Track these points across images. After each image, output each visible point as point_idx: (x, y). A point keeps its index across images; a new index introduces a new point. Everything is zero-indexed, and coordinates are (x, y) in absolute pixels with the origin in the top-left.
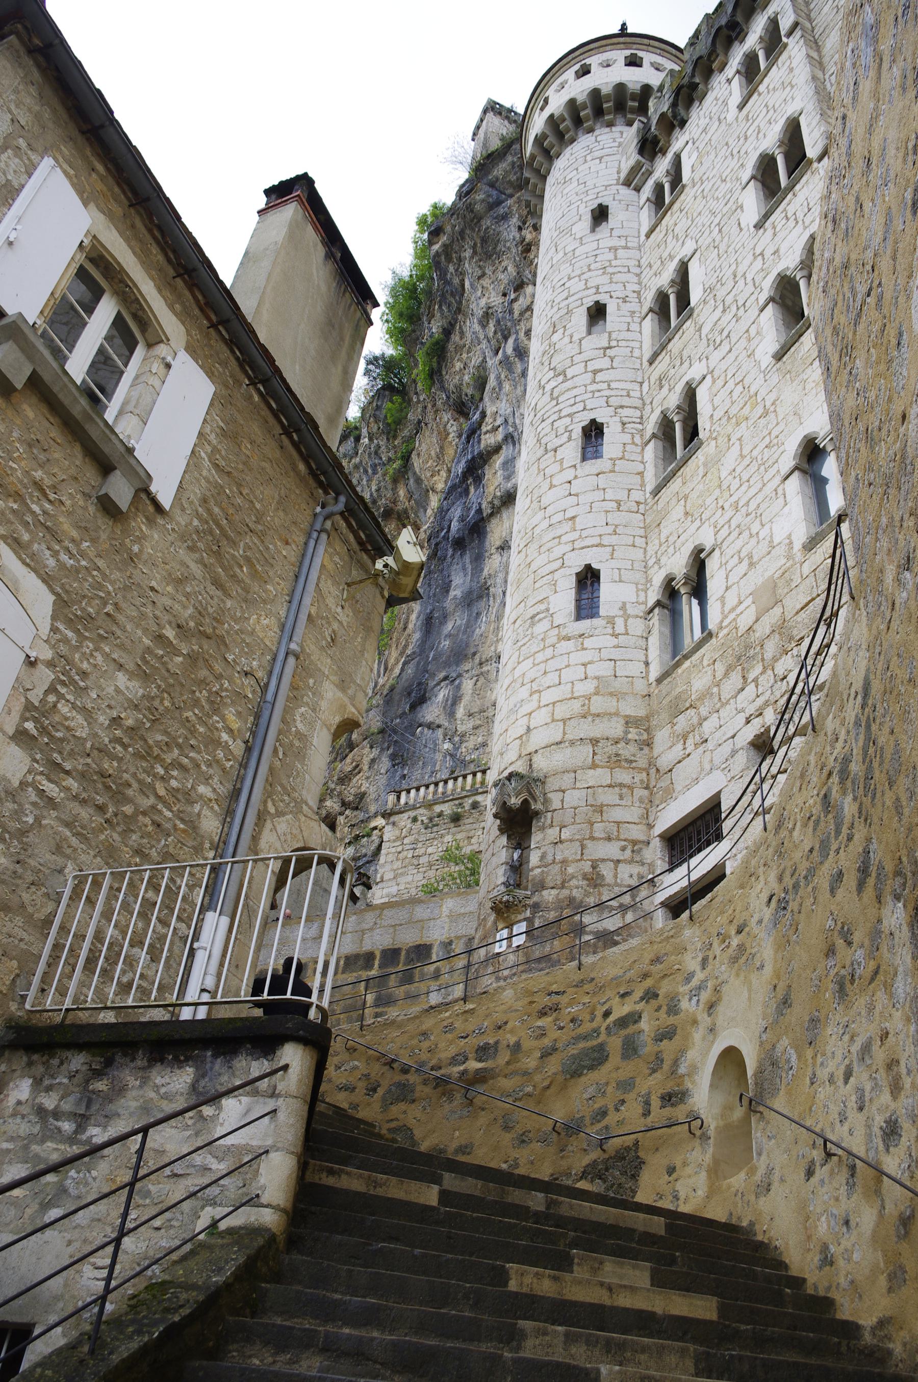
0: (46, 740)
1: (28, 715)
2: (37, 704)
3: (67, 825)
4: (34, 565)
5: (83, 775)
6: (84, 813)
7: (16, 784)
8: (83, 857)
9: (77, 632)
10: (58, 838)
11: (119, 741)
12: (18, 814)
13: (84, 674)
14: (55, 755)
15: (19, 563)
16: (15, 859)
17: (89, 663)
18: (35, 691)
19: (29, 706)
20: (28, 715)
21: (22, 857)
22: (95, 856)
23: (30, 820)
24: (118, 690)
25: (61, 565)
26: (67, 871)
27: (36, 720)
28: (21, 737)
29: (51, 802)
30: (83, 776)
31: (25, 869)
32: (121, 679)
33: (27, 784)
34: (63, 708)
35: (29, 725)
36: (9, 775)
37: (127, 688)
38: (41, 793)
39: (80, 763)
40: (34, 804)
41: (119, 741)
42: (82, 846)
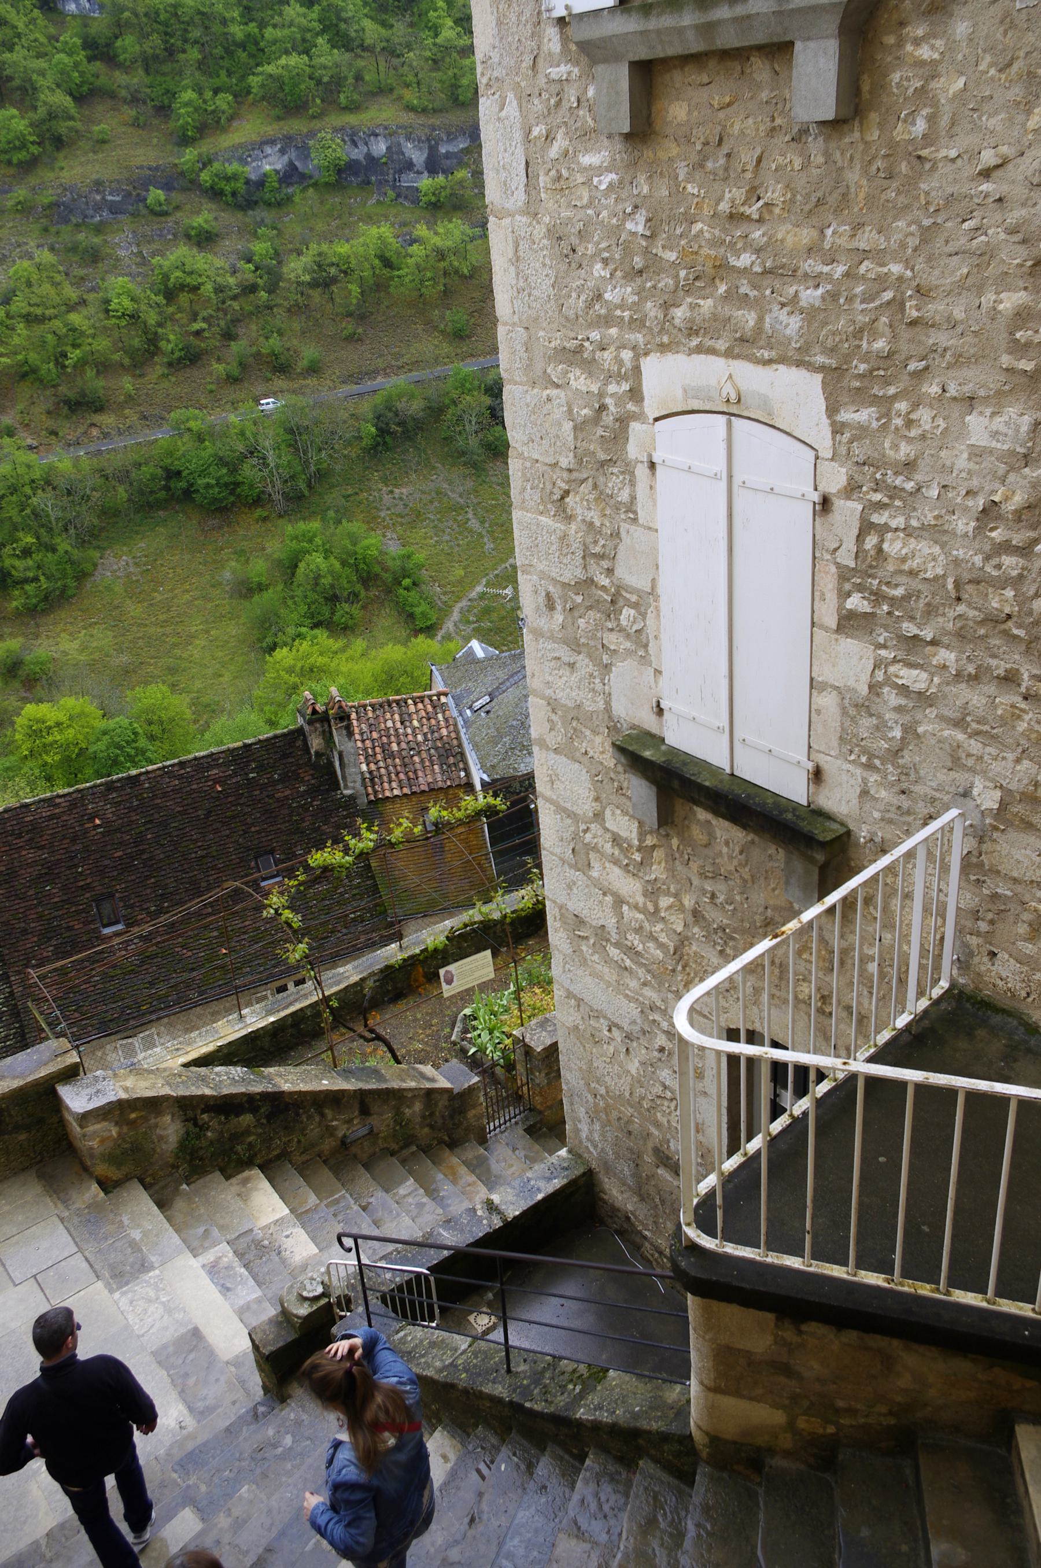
0: (885, 608)
1: (847, 586)
2: (852, 565)
3: (959, 723)
4: (34, 803)
5: (961, 635)
6: (976, 698)
7: (864, 690)
8: (996, 767)
9: (876, 401)
10: (947, 747)
11: (1006, 548)
12: (881, 727)
13: (909, 466)
14: (905, 625)
15: (759, 370)
16: (896, 789)
17: (910, 440)
18: (844, 547)
19: (844, 574)
20: (847, 586)
21: (904, 785)
22: (1018, 761)
23: (897, 733)
24: (977, 453)
25: (810, 314)
26: (975, 792)
27: (860, 588)
28: (849, 623)
29: (924, 699)
30: (962, 636)
31: (915, 801)
32: (978, 427)
33: (881, 685)
34: (893, 546)
35: (856, 602)
36: (851, 683)
37: (995, 435)
38: (904, 690)
39: (946, 622)
40: (899, 709)
41: (1006, 548)
42: (988, 749)
